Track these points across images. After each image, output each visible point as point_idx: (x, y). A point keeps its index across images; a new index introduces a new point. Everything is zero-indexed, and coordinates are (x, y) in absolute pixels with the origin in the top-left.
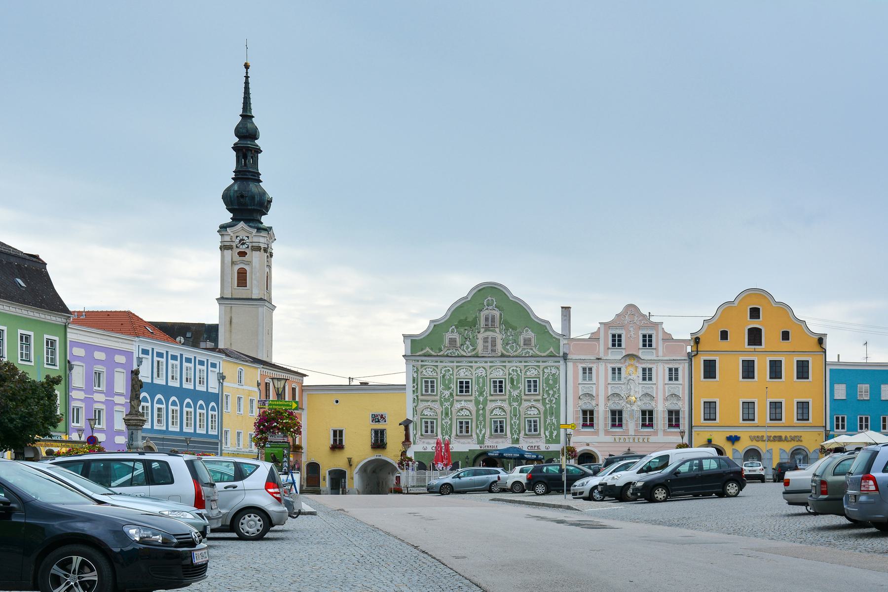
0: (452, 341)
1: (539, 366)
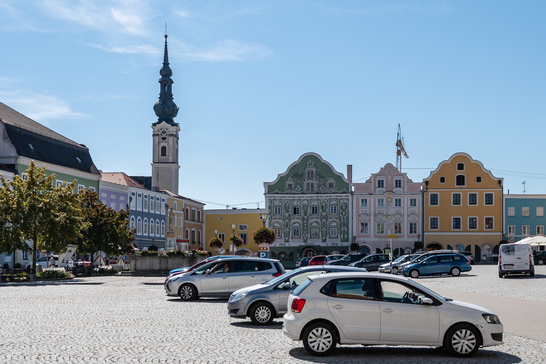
0: (290, 185)
1: (337, 199)
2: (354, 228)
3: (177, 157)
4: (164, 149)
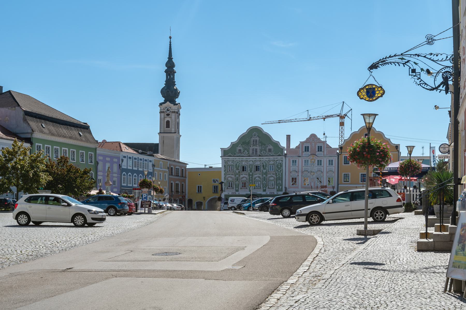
0: (240, 150)
2: (287, 182)
3: (178, 128)
4: (168, 123)
